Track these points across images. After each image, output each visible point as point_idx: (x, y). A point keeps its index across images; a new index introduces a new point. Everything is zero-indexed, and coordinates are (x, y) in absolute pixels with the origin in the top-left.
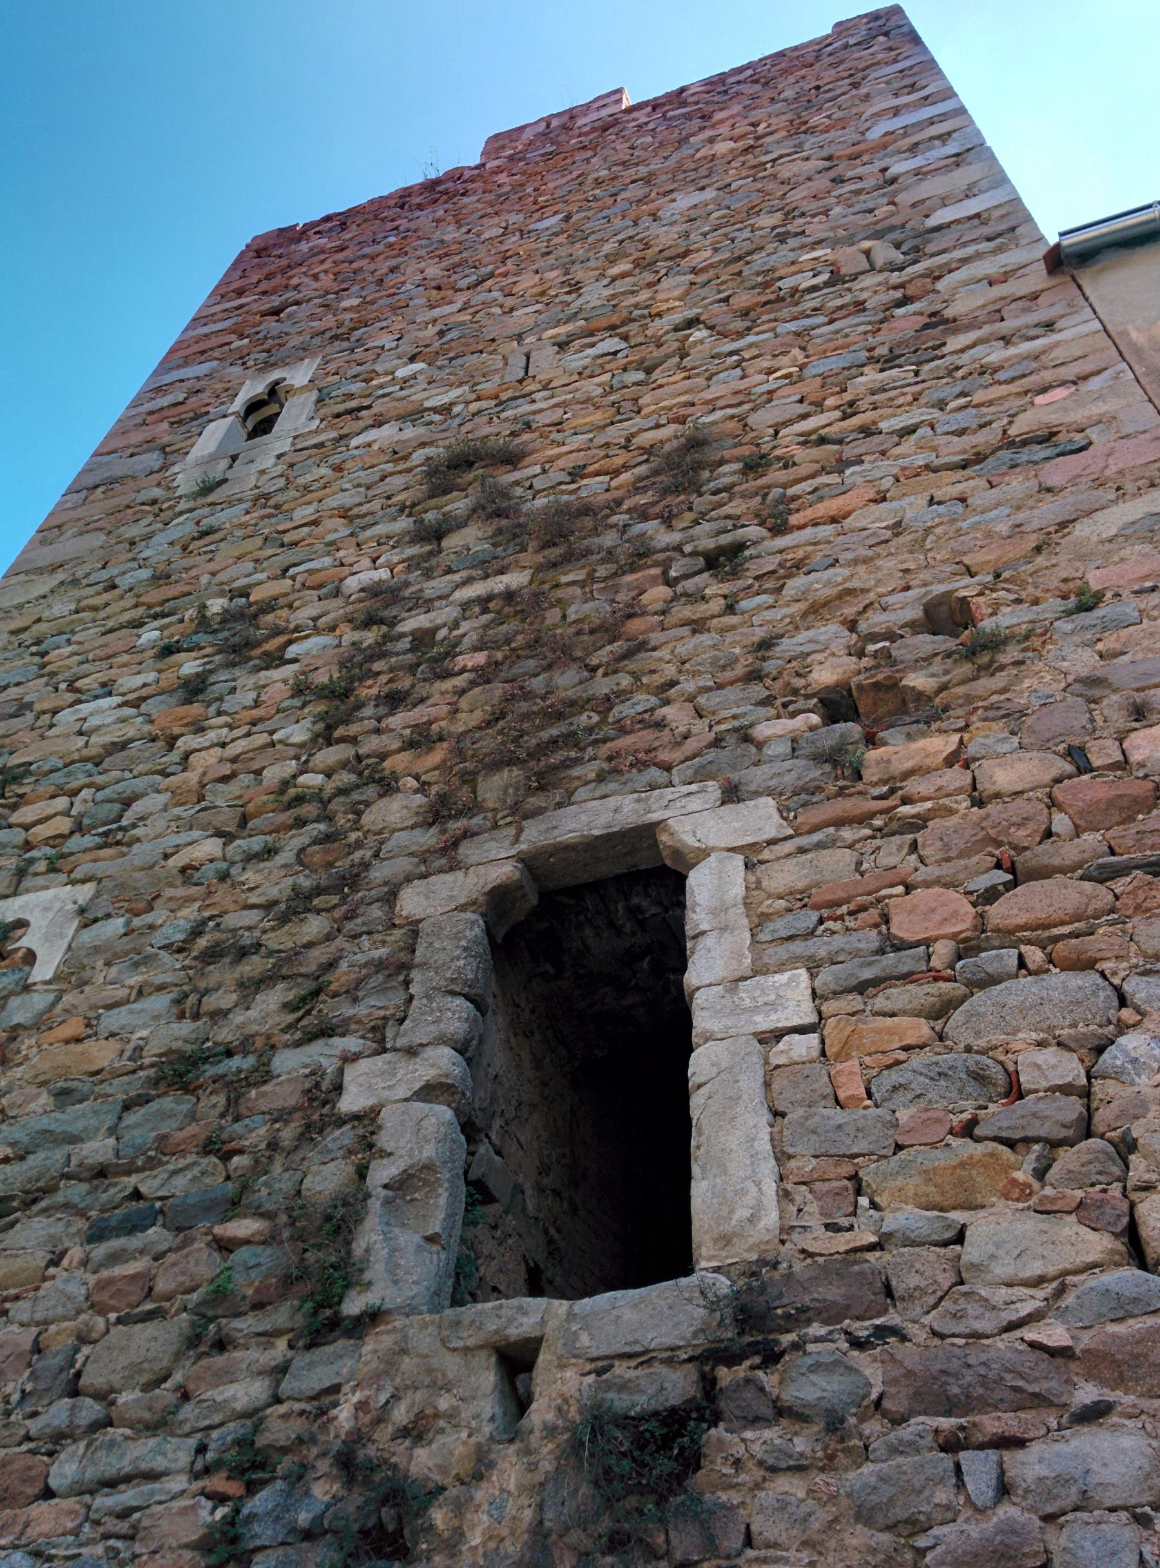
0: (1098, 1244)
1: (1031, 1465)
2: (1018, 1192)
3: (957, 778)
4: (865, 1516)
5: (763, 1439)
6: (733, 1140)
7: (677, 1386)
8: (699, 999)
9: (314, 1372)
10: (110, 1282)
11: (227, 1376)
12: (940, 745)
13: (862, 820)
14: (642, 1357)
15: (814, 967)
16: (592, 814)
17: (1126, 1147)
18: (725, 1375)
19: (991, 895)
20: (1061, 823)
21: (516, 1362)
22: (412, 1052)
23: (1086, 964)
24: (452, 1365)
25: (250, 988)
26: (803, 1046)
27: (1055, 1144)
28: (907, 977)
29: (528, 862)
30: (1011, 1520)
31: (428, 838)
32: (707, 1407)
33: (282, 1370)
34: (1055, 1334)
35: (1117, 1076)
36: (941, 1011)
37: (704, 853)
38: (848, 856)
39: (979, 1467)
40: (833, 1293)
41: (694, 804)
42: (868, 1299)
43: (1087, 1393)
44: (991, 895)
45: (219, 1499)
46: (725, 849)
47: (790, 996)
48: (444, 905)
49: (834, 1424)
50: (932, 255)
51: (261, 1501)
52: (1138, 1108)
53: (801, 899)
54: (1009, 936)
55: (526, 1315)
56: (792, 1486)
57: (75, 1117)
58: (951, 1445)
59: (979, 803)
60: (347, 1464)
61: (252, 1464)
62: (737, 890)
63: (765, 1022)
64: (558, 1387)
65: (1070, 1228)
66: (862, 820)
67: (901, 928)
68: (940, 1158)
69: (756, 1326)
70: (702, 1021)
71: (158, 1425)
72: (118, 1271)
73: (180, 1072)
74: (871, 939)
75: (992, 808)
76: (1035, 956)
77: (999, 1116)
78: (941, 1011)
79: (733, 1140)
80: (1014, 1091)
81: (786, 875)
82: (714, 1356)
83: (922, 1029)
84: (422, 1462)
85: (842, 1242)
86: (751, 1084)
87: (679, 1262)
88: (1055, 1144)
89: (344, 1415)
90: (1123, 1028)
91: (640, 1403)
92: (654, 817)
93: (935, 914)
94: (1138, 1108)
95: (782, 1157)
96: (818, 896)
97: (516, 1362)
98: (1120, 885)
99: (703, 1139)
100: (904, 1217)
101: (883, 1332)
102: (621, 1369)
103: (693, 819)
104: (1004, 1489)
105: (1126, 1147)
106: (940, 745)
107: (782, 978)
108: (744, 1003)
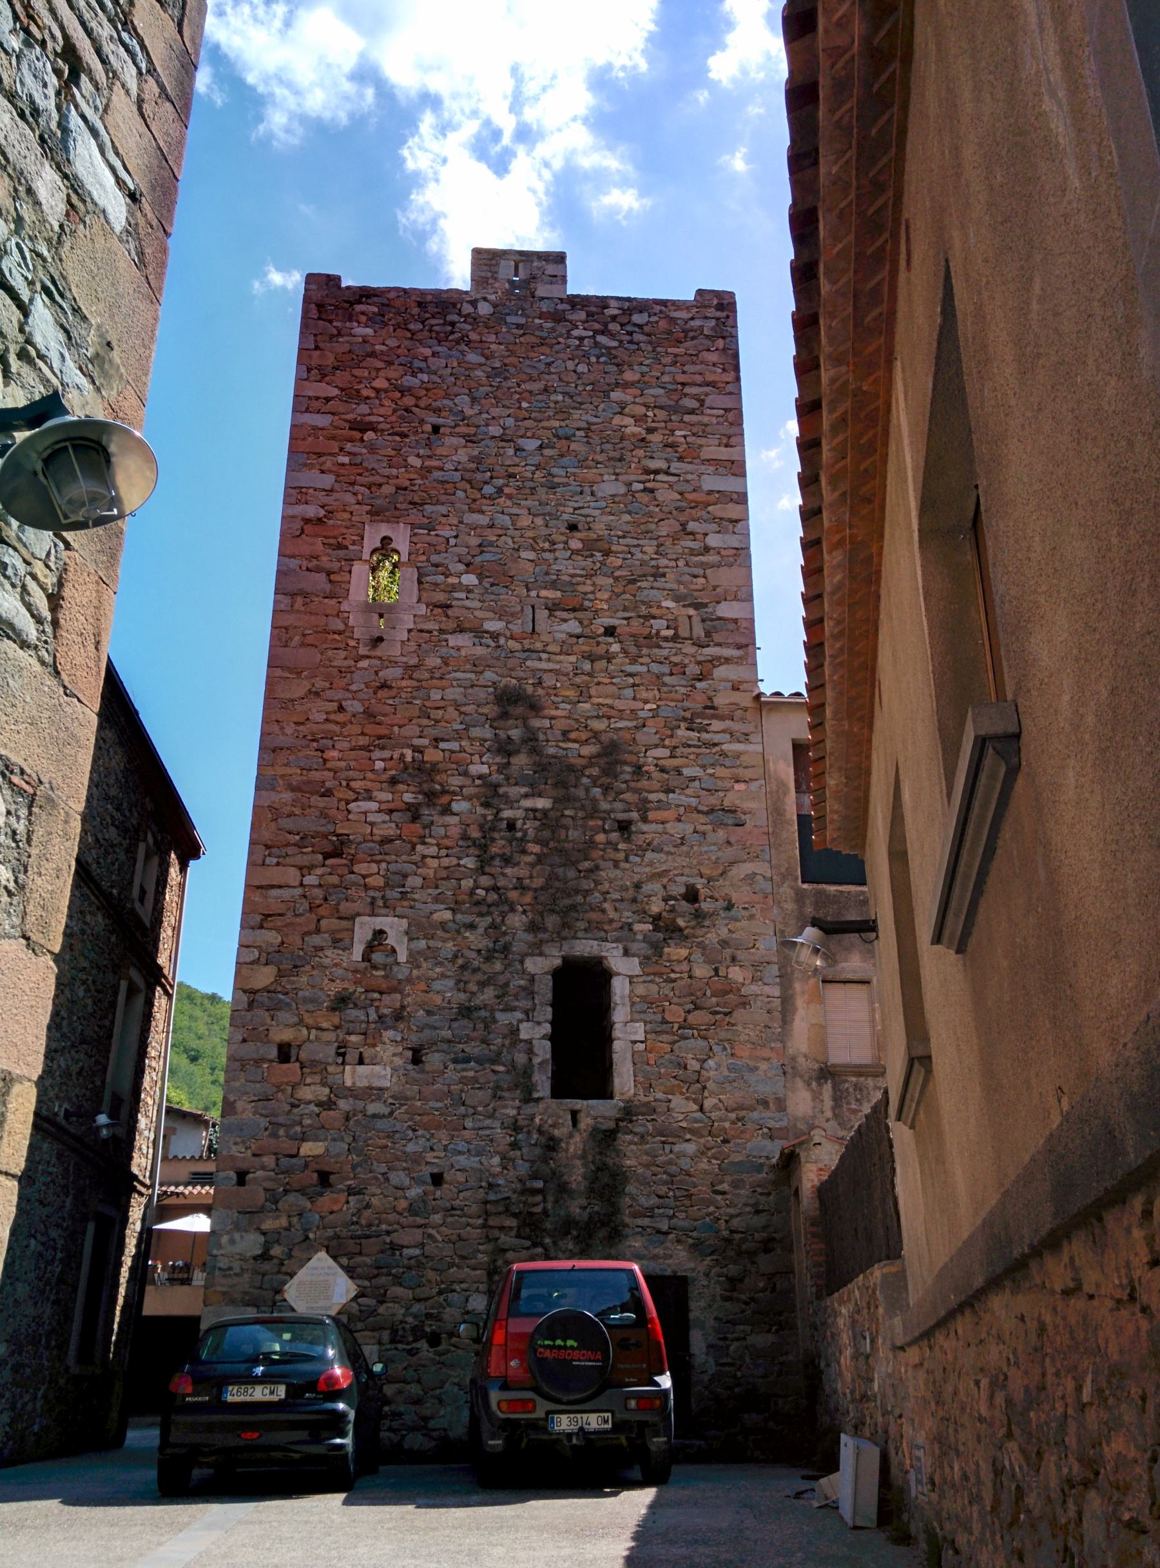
0: (696, 1107)
1: (677, 1148)
2: (682, 1093)
3: (685, 967)
4: (647, 1154)
7: (611, 1125)
8: (617, 1026)
9: (529, 1109)
11: (505, 1107)
12: (684, 952)
14: (605, 1118)
15: (645, 1022)
16: (585, 947)
17: (704, 1088)
22: (539, 1023)
23: (705, 1038)
25: (482, 985)
26: (642, 1046)
30: (632, 1271)
31: (530, 937)
33: (519, 1108)
34: (684, 1124)
39: (667, 1147)
40: (644, 1110)
41: (615, 953)
43: (688, 1136)
44: (689, 1012)
46: (623, 967)
48: (541, 966)
49: (642, 1137)
50: (719, 645)
52: (709, 1079)
55: (578, 1104)
56: (634, 1147)
58: (664, 1142)
59: (690, 977)
60: (540, 1131)
61: (516, 1128)
62: (627, 992)
63: (634, 1038)
64: (585, 1122)
65: (691, 1104)
67: (668, 1017)
69: (628, 1112)
70: (617, 1033)
71: (491, 1116)
73: (466, 1012)
74: (659, 1017)
81: (640, 990)
82: (618, 1120)
84: (556, 1133)
86: (629, 1056)
87: (611, 1097)
89: (537, 1120)
91: (604, 1127)
93: (675, 1013)
94: (709, 1079)
97: (574, 1114)
99: (617, 63)
100: (660, 1096)
105: (704, 1088)
106: (684, 952)
108: (627, 1032)
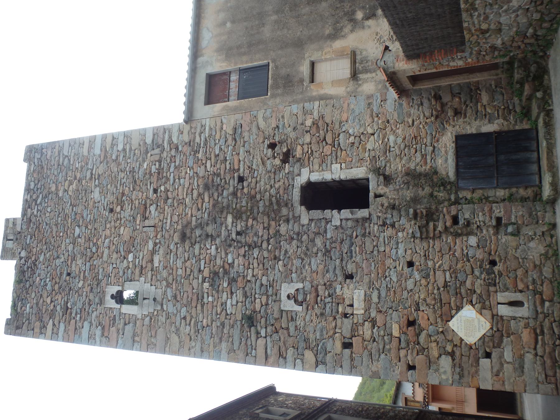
1: (392, 145)
4: (395, 159)
5: (387, 168)
6: (355, 172)
7: (381, 178)
10: (359, 252)
13: (309, 158)
15: (332, 164)
16: (296, 195)
18: (381, 173)
19: (327, 143)
20: (317, 135)
21: (377, 196)
23: (339, 135)
24: (376, 203)
26: (343, 165)
27: (361, 140)
28: (336, 153)
29: (301, 205)
32: (384, 175)
34: (380, 142)
35: (354, 133)
36: (341, 150)
37: (309, 178)
38: (315, 159)
39: (392, 149)
40: (374, 162)
42: (374, 159)
43: (386, 140)
44: (327, 143)
45: (388, 227)
46: (306, 175)
47: (336, 167)
51: (388, 223)
53: (320, 165)
54: (334, 141)
56: (392, 165)
57: (331, 269)
58: (390, 151)
65: (370, 139)
66: (309, 158)
68: (361, 151)
69: (378, 171)
72: (358, 252)
75: (312, 142)
76: (337, 139)
77: (356, 144)
78: (341, 150)
79: (355, 172)
80: (353, 143)
81: (316, 167)
83: (344, 152)
85: (369, 161)
86: (348, 171)
88: (361, 140)
90: (348, 132)
92: (300, 186)
93: (328, 150)
95: (357, 167)
96: (321, 163)
97: (377, 196)
98: (329, 129)
100: (367, 154)
101: (378, 157)
102: (379, 183)
103: (302, 180)
104: (394, 147)
106: (299, 147)
107: (333, 167)
108: (336, 172)
